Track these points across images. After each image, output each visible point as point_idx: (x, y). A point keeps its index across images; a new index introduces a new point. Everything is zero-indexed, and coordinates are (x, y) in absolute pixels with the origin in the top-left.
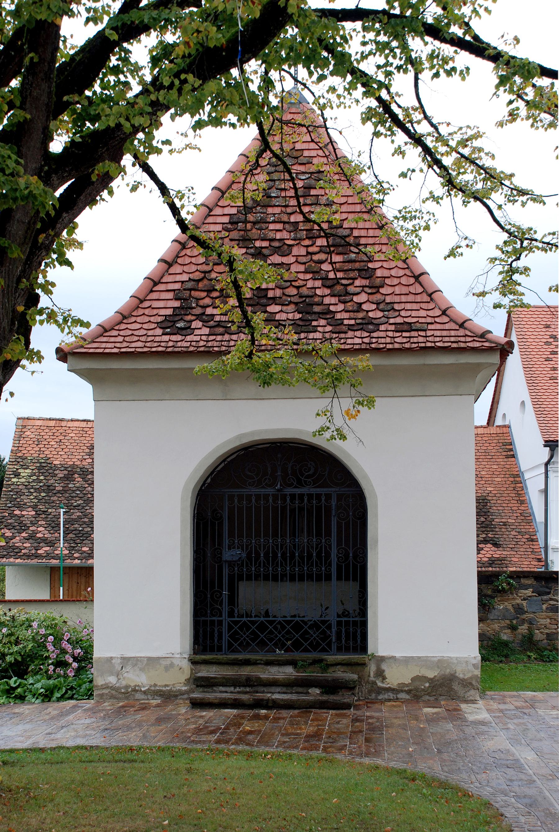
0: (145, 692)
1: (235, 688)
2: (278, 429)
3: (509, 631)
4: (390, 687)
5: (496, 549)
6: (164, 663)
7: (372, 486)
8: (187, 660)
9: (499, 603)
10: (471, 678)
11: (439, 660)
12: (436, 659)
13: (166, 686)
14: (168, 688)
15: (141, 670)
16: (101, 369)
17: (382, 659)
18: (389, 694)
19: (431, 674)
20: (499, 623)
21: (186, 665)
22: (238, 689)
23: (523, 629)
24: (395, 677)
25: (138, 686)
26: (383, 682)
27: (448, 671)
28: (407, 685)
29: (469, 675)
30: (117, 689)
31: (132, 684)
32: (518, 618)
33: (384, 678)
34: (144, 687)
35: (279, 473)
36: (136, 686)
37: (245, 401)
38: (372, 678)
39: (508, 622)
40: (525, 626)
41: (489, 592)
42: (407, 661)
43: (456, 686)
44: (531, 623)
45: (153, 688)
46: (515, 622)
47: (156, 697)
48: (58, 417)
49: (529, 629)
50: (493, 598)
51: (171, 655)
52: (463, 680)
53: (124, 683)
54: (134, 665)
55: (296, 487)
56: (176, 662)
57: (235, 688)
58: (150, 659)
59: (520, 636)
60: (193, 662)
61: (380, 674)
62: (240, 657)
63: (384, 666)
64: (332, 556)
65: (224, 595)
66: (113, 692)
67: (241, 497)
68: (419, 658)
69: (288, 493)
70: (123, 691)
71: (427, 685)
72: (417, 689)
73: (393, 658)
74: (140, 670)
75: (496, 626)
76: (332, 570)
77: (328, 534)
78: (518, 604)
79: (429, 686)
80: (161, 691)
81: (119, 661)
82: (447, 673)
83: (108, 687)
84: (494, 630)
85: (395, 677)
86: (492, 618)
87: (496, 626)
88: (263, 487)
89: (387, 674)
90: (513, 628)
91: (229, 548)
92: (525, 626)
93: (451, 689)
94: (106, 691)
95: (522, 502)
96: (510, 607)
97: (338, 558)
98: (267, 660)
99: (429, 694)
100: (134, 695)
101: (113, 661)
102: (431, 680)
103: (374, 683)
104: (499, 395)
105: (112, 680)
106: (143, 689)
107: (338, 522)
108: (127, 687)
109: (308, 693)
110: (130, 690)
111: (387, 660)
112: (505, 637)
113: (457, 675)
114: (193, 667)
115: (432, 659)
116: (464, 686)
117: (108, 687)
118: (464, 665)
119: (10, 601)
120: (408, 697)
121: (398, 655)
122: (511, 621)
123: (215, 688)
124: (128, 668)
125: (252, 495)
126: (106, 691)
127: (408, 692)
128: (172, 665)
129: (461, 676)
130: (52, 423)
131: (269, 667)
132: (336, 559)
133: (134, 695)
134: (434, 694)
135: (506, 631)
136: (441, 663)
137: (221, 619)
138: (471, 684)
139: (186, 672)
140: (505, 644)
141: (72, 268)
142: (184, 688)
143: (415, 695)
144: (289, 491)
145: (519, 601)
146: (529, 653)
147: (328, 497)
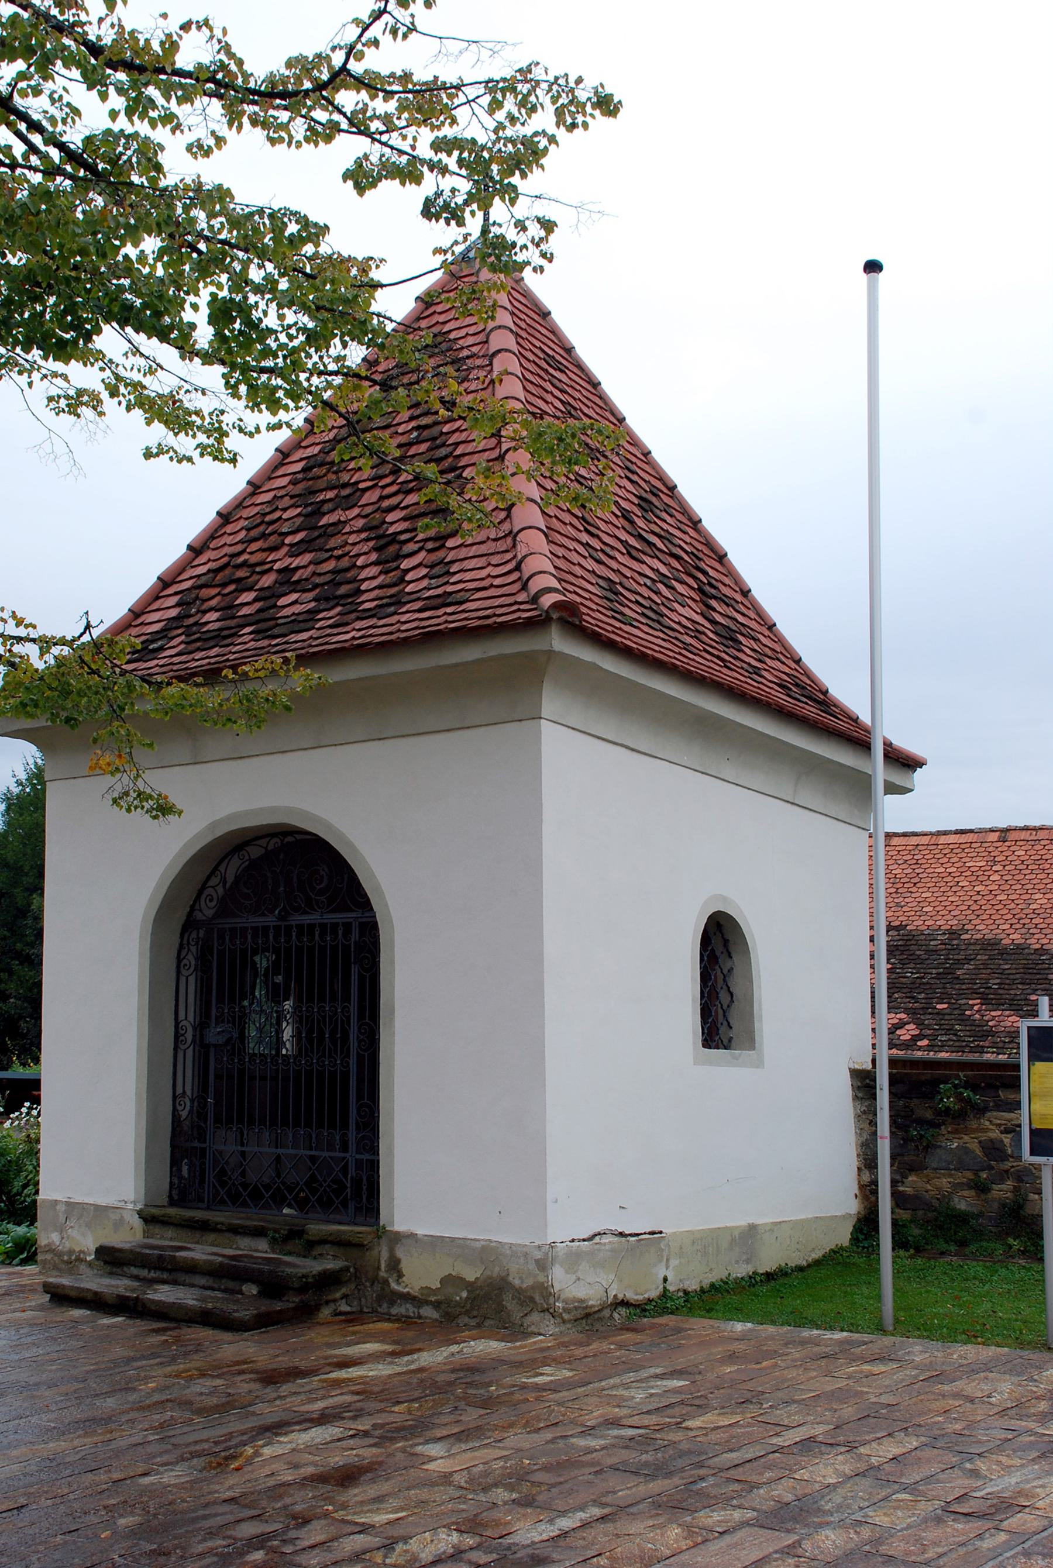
1: (149, 1272)
2: (262, 809)
3: (973, 1193)
4: (408, 1293)
6: (114, 1216)
7: (387, 905)
9: (951, 1136)
10: (533, 1287)
11: (483, 1246)
12: (478, 1245)
15: (88, 1225)
17: (397, 1238)
18: (408, 1306)
19: (471, 1275)
20: (951, 1176)
23: (1003, 1191)
24: (419, 1274)
25: (83, 1252)
26: (399, 1284)
27: (497, 1269)
28: (435, 1292)
29: (529, 1282)
30: (59, 1254)
32: (992, 1168)
33: (400, 1275)
36: (81, 1252)
37: (221, 763)
38: (383, 1274)
39: (969, 1175)
40: (1009, 1184)
41: (929, 1115)
42: (435, 1243)
43: (510, 1303)
44: (1019, 1179)
46: (984, 1175)
48: (934, 830)
49: (1016, 1190)
50: (939, 1126)
51: (120, 1205)
52: (519, 1291)
53: (67, 1245)
55: (305, 913)
57: (149, 1272)
58: (97, 1207)
59: (996, 1205)
60: (148, 1219)
61: (394, 1265)
62: (198, 1214)
63: (400, 1253)
64: (351, 1036)
68: (453, 1239)
69: (293, 923)
71: (464, 1294)
72: (448, 1302)
73: (412, 1236)
75: (944, 1182)
76: (351, 1063)
77: (347, 998)
78: (991, 1140)
79: (467, 1298)
82: (495, 1275)
84: (939, 1189)
85: (419, 1274)
86: (934, 1165)
87: (944, 1182)
89: (404, 1266)
90: (982, 1189)
91: (217, 1024)
92: (1009, 1184)
93: (501, 1309)
96: (974, 1146)
97: (359, 1042)
98: (230, 1224)
99: (467, 1313)
101: (58, 1208)
102: (470, 1286)
103: (386, 1282)
104: (706, 730)
105: (55, 1237)
107: (359, 973)
108: (71, 1252)
109: (241, 1292)
111: (403, 1241)
112: (962, 1206)
113: (510, 1279)
115: (473, 1244)
116: (522, 1304)
118: (522, 1261)
120: (435, 1315)
121: (420, 1231)
122: (976, 1173)
123: (125, 1269)
125: (247, 928)
127: (437, 1305)
129: (517, 1282)
130: (925, 840)
131: (238, 1237)
132: (356, 1044)
134: (475, 1313)
135: (966, 1193)
136: (488, 1252)
137: (204, 1145)
138: (532, 1299)
140: (962, 1219)
143: (447, 1313)
144: (297, 919)
145: (995, 1134)
146: (1011, 1241)
147: (347, 927)
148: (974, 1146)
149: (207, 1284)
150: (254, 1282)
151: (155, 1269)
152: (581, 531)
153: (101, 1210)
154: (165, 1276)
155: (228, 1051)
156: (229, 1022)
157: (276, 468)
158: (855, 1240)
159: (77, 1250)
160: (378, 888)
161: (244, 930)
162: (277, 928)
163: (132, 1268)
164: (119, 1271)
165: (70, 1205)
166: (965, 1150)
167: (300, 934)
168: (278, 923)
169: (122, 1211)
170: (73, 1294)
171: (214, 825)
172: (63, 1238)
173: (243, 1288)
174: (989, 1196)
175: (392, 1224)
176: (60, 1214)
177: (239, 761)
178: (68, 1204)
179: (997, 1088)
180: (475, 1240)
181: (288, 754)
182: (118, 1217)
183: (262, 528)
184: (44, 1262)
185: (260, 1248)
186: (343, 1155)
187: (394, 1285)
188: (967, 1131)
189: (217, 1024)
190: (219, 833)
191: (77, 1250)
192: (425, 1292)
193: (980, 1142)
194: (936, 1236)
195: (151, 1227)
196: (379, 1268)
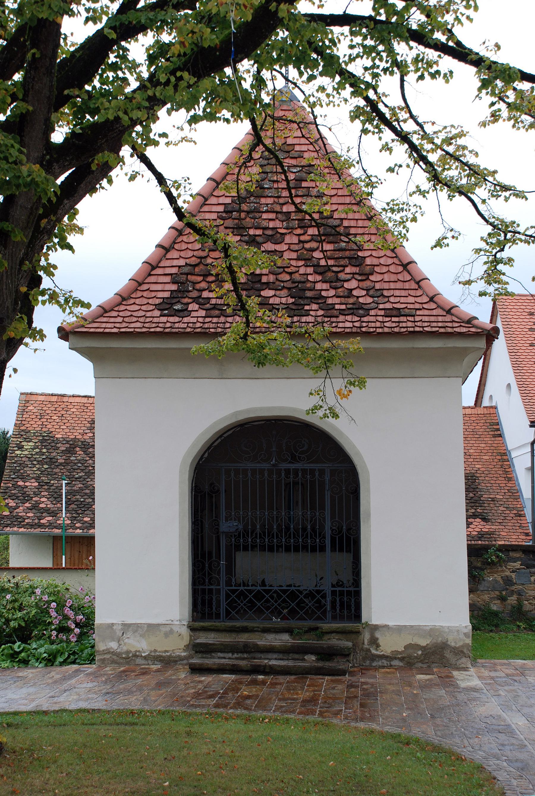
0: (145, 658)
1: (233, 654)
3: (499, 601)
4: (383, 655)
9: (489, 575)
10: (462, 646)
12: (428, 628)
14: (168, 654)
17: (376, 627)
19: (423, 642)
20: (489, 594)
21: (185, 631)
22: (236, 655)
23: (512, 600)
24: (389, 645)
25: (139, 651)
26: (377, 650)
27: (440, 639)
28: (400, 653)
30: (118, 655)
31: (133, 650)
33: (378, 646)
34: (144, 652)
36: (136, 651)
38: (366, 646)
39: (497, 593)
41: (479, 565)
42: (400, 629)
43: (448, 654)
44: (519, 594)
45: (153, 654)
47: (156, 663)
49: (518, 600)
50: (483, 570)
51: (170, 622)
53: (125, 648)
54: (135, 632)
56: (176, 629)
58: (150, 625)
59: (510, 607)
60: (192, 629)
61: (374, 642)
62: (238, 624)
63: (377, 635)
65: (221, 565)
66: (115, 657)
68: (412, 626)
70: (124, 656)
71: (420, 652)
72: (410, 657)
75: (486, 597)
76: (327, 542)
77: (322, 507)
79: (422, 654)
81: (120, 627)
82: (439, 642)
83: (109, 653)
84: (484, 601)
85: (389, 645)
86: (482, 589)
87: (486, 597)
88: (259, 462)
89: (381, 641)
90: (503, 599)
91: (227, 520)
94: (107, 656)
95: (510, 479)
96: (499, 579)
99: (422, 662)
101: (115, 627)
103: (369, 650)
105: (113, 645)
108: (128, 652)
109: (304, 659)
111: (380, 629)
112: (495, 608)
114: (192, 634)
115: (425, 628)
116: (456, 654)
117: (109, 653)
118: (456, 633)
119: (14, 569)
121: (391, 624)
124: (129, 634)
125: (315, 469)
126: (107, 656)
127: (402, 659)
128: (171, 631)
129: (453, 644)
131: (266, 634)
134: (427, 661)
135: (496, 602)
136: (432, 631)
137: (218, 587)
138: (462, 652)
140: (496, 614)
141: (73, 252)
142: (183, 654)
145: (508, 573)
147: (322, 472)
148: (499, 579)
150: (312, 653)
151: (242, 652)
155: (235, 536)
156: (235, 520)
157: (201, 207)
160: (358, 453)
165: (126, 627)
166: (496, 581)
170: (215, 667)
172: (120, 645)
174: (506, 603)
175: (371, 621)
178: (124, 625)
179: (509, 551)
184: (103, 660)
187: (374, 651)
188: (496, 572)
189: (227, 520)
190: (241, 418)
192: (395, 653)
193: (502, 577)
194: (484, 623)
196: (363, 644)
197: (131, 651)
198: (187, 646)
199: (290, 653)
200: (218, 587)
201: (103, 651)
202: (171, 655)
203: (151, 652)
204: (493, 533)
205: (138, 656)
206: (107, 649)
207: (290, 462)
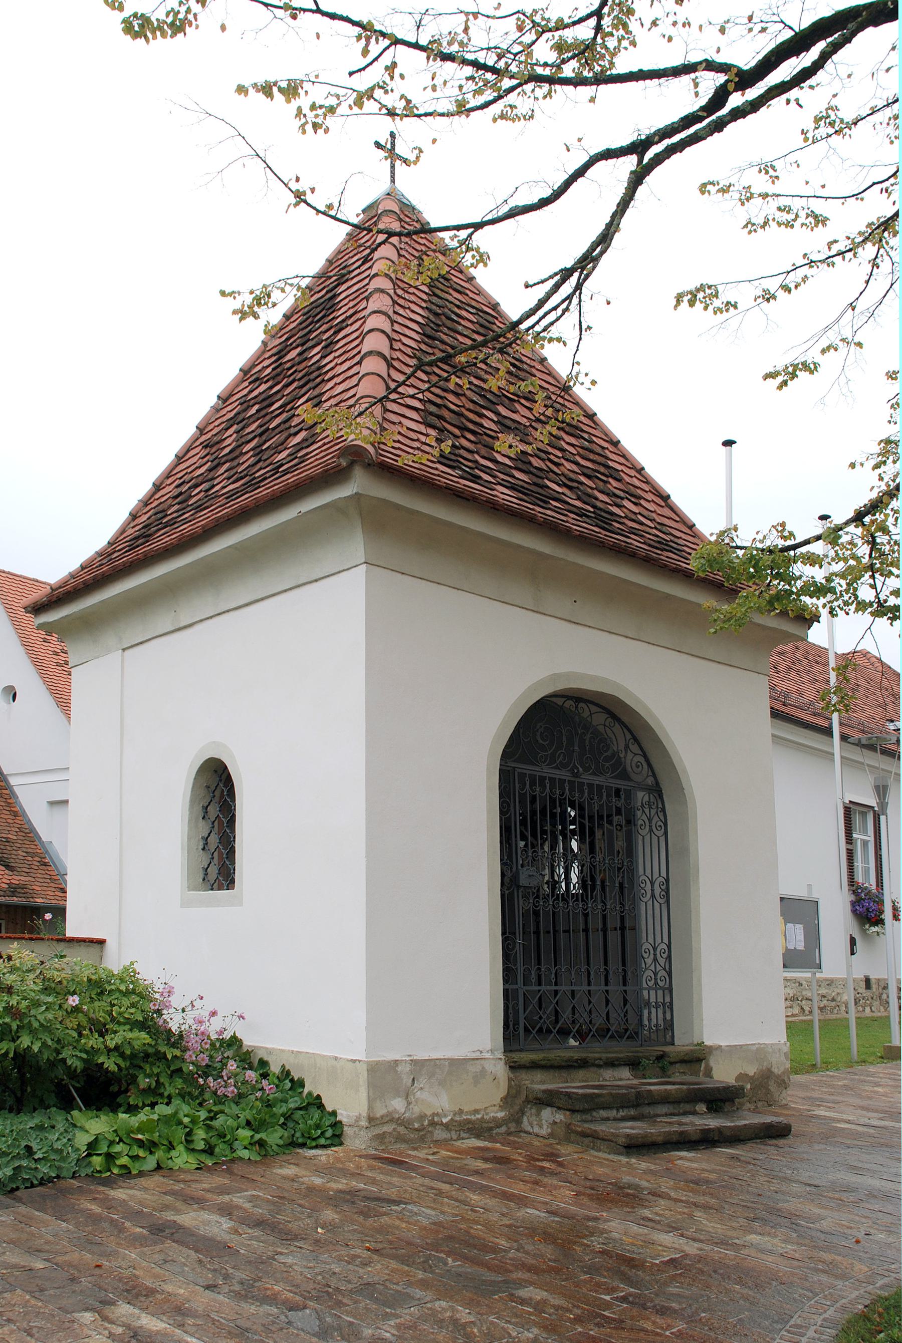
0: (447, 1127)
1: (618, 1111)
5: (11, 873)
6: (474, 1069)
8: (503, 1062)
12: (754, 1048)
13: (476, 1111)
14: (479, 1116)
15: (442, 1083)
16: (398, 507)
19: (751, 1070)
21: (500, 1070)
22: (622, 1113)
25: (437, 1114)
27: (765, 1064)
31: (429, 1113)
34: (445, 1116)
35: (576, 748)
36: (434, 1114)
45: (457, 1118)
47: (463, 1135)
51: (474, 1056)
53: (417, 1110)
54: (431, 1075)
56: (489, 1067)
57: (618, 1111)
58: (453, 1062)
60: (514, 1067)
65: (517, 946)
66: (401, 1129)
67: (533, 778)
70: (416, 1125)
74: (440, 1084)
80: (469, 1121)
81: (408, 1068)
83: (392, 1120)
88: (557, 768)
94: (388, 1128)
95: (16, 814)
98: (607, 1058)
100: (431, 1132)
101: (399, 1069)
106: (444, 1121)
108: (422, 1117)
110: (426, 1123)
111: (714, 1052)
114: (512, 1076)
117: (392, 1120)
119: (72, 940)
121: (723, 1043)
123: (594, 1114)
124: (422, 1082)
126: (388, 1128)
128: (483, 1071)
133: (431, 1132)
134: (754, 1099)
137: (515, 987)
139: (502, 1083)
141: (676, 307)
142: (501, 1115)
149: (668, 1112)
151: (623, 1107)
152: (662, 507)
153: (457, 1065)
154: (632, 1112)
155: (534, 893)
158: (530, 1018)
159: (429, 1113)
161: (542, 779)
162: (571, 783)
163: (601, 1112)
164: (588, 1117)
165: (418, 1065)
167: (533, 783)
168: (573, 779)
169: (482, 1062)
170: (660, 1139)
171: (554, 677)
173: (697, 1108)
176: (404, 1076)
177: (574, 625)
178: (414, 1062)
180: (752, 1044)
181: (614, 636)
182: (478, 1068)
183: (310, 319)
185: (623, 1077)
186: (539, 988)
191: (429, 1113)
195: (518, 1074)
197: (426, 1115)
198: (505, 1099)
199: (680, 1102)
200: (515, 987)
201: (382, 1117)
202: (483, 1118)
203: (454, 1115)
204: (23, 887)
205: (437, 1124)
206: (389, 1114)
207: (594, 774)
